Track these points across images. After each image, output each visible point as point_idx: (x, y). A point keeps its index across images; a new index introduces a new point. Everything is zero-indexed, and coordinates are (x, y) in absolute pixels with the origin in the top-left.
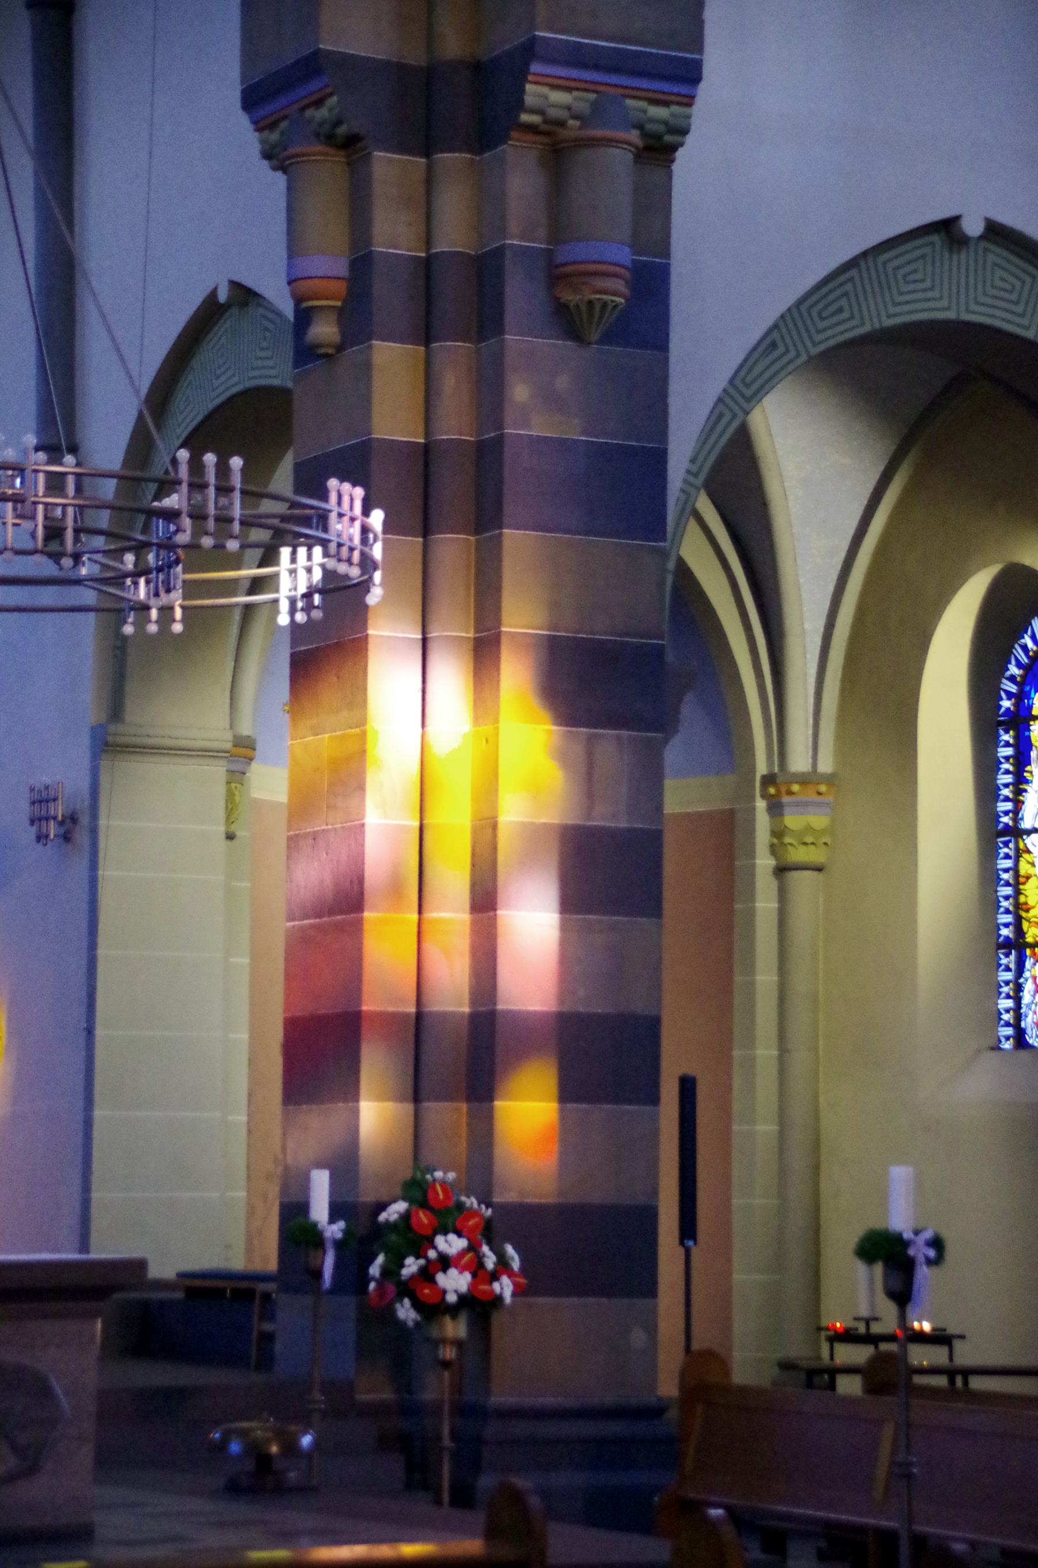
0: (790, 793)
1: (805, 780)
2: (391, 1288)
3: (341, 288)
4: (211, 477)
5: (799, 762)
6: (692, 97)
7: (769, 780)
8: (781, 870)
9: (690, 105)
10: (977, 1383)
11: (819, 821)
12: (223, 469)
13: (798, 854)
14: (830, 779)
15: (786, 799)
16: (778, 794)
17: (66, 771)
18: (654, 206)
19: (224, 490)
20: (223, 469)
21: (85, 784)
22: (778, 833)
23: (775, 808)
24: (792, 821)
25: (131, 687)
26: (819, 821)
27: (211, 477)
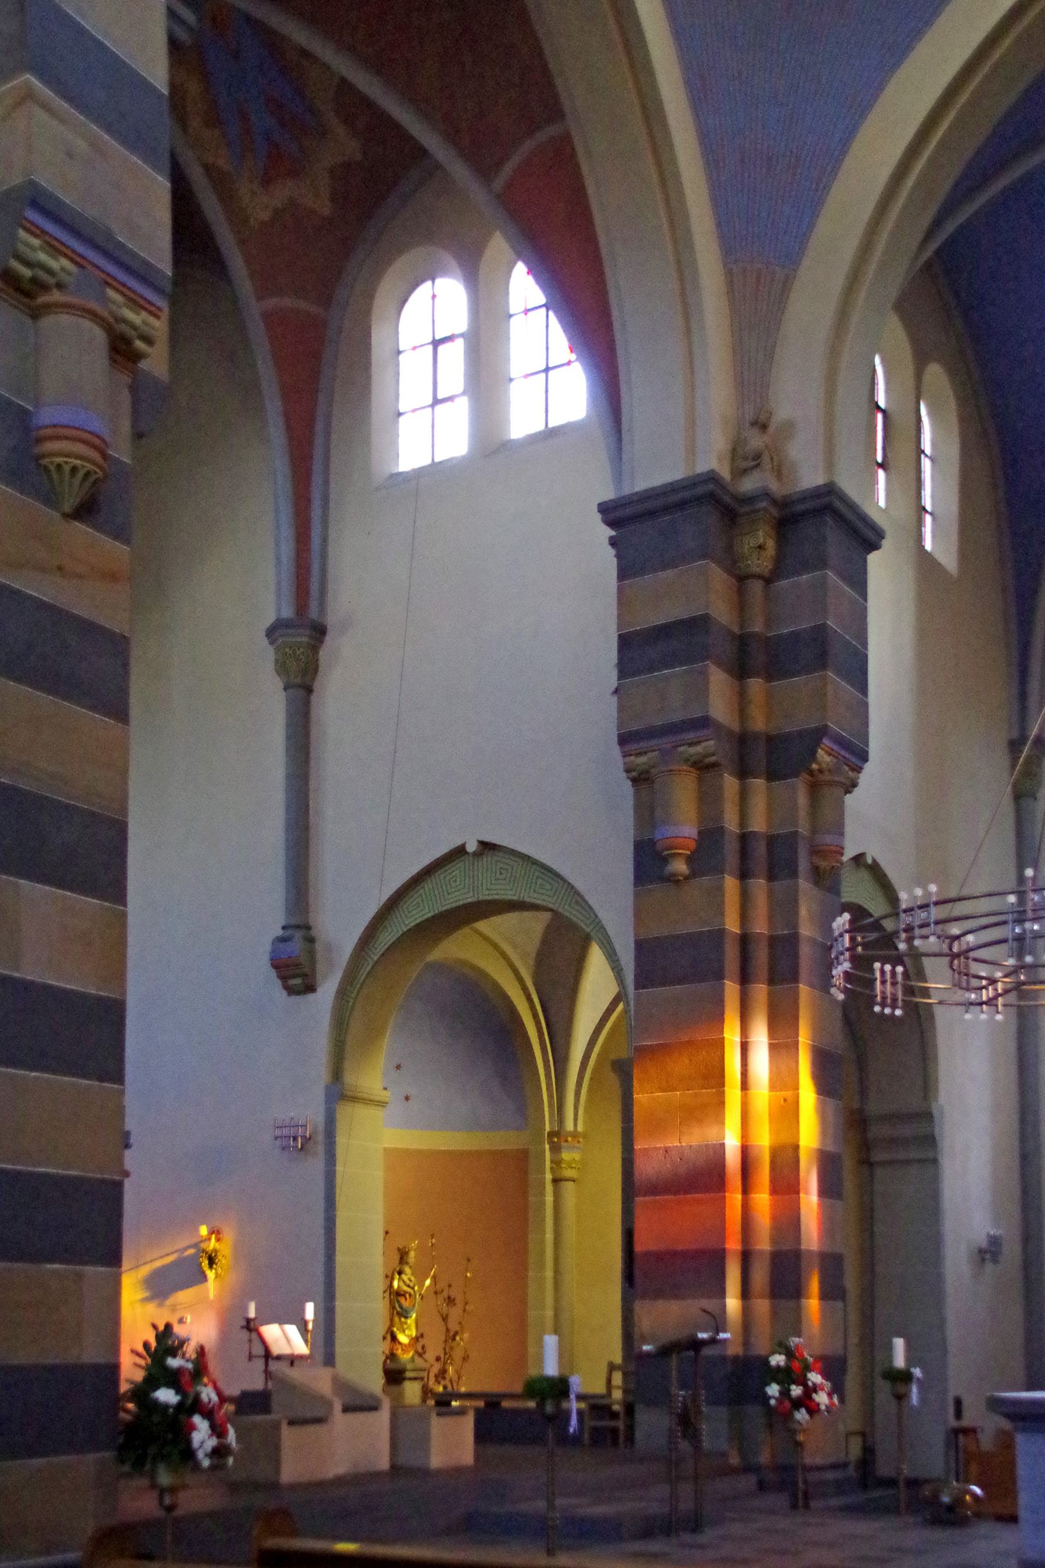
0: (566, 1141)
1: (575, 1135)
2: (787, 1404)
3: (693, 845)
4: (888, 976)
5: (569, 1126)
6: (862, 768)
7: (551, 1134)
8: (556, 1181)
9: (859, 772)
10: (506, 1404)
11: (577, 1156)
12: (893, 973)
13: (569, 1173)
14: (585, 1135)
15: (564, 1144)
16: (559, 1142)
17: (310, 1112)
18: (648, 813)
19: (894, 984)
20: (893, 973)
21: (320, 1119)
22: (557, 1163)
23: (556, 1149)
24: (566, 1156)
25: (347, 1064)
26: (577, 1156)
27: (888, 976)
